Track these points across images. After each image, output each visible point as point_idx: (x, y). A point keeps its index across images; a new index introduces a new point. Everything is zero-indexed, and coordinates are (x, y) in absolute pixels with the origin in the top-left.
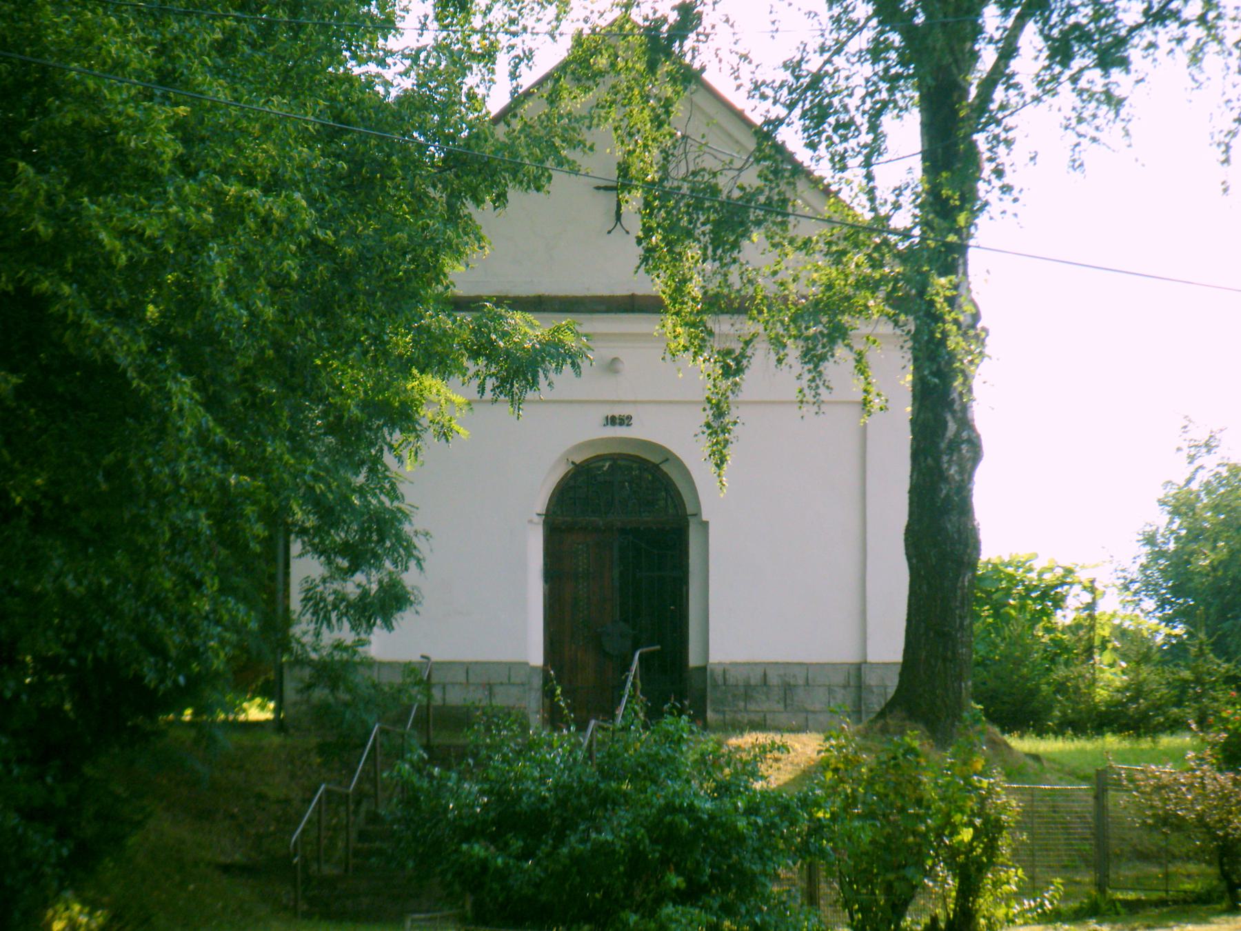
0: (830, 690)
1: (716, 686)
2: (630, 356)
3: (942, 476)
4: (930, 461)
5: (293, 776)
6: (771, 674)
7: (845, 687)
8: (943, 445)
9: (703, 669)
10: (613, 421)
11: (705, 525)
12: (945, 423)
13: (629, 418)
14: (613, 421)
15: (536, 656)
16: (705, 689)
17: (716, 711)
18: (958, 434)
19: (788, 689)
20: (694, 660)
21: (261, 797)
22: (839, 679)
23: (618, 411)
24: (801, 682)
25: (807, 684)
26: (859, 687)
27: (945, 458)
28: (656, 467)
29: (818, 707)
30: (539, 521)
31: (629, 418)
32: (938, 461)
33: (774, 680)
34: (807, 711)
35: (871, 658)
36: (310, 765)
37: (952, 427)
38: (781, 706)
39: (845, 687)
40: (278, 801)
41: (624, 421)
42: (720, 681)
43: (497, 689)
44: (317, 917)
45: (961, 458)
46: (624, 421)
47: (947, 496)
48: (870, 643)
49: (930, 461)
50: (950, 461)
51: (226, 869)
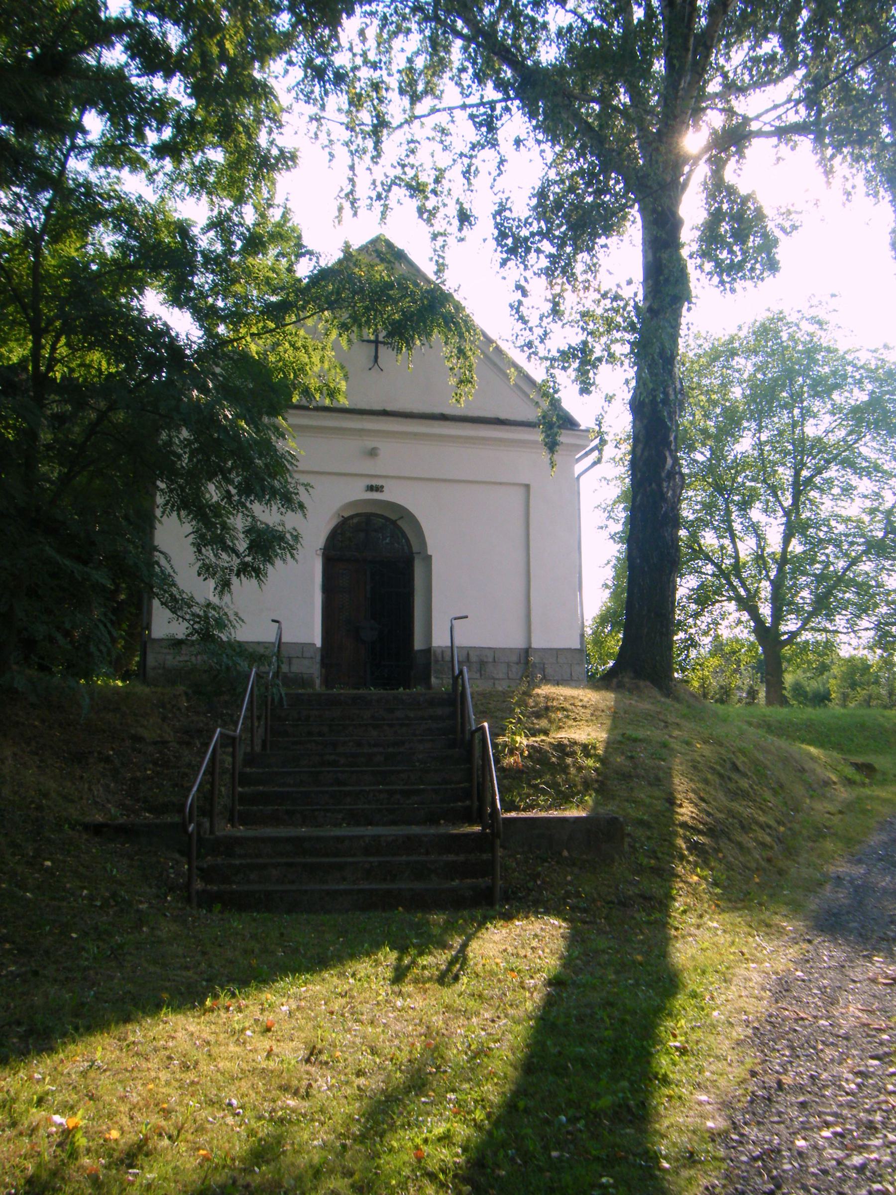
0: (508, 665)
1: (437, 661)
2: (385, 447)
3: (663, 497)
4: (654, 485)
5: (164, 719)
6: (471, 654)
7: (517, 664)
8: (663, 475)
9: (428, 651)
10: (371, 488)
11: (428, 559)
12: (665, 458)
13: (382, 487)
14: (371, 488)
15: (318, 640)
16: (430, 664)
17: (437, 678)
18: (673, 467)
19: (482, 664)
20: (418, 644)
21: (138, 739)
22: (514, 658)
23: (375, 482)
24: (491, 660)
25: (494, 661)
26: (527, 662)
27: (665, 484)
28: (394, 523)
29: (501, 676)
30: (320, 553)
31: (382, 487)
32: (660, 486)
33: (473, 658)
34: (494, 679)
35: (535, 645)
36: (179, 709)
37: (669, 461)
38: (478, 675)
39: (517, 664)
40: (155, 743)
41: (378, 489)
42: (440, 658)
43: (294, 661)
44: (253, 983)
45: (674, 485)
46: (378, 489)
47: (666, 512)
48: (533, 635)
49: (654, 485)
50: (668, 487)
51: (97, 830)
